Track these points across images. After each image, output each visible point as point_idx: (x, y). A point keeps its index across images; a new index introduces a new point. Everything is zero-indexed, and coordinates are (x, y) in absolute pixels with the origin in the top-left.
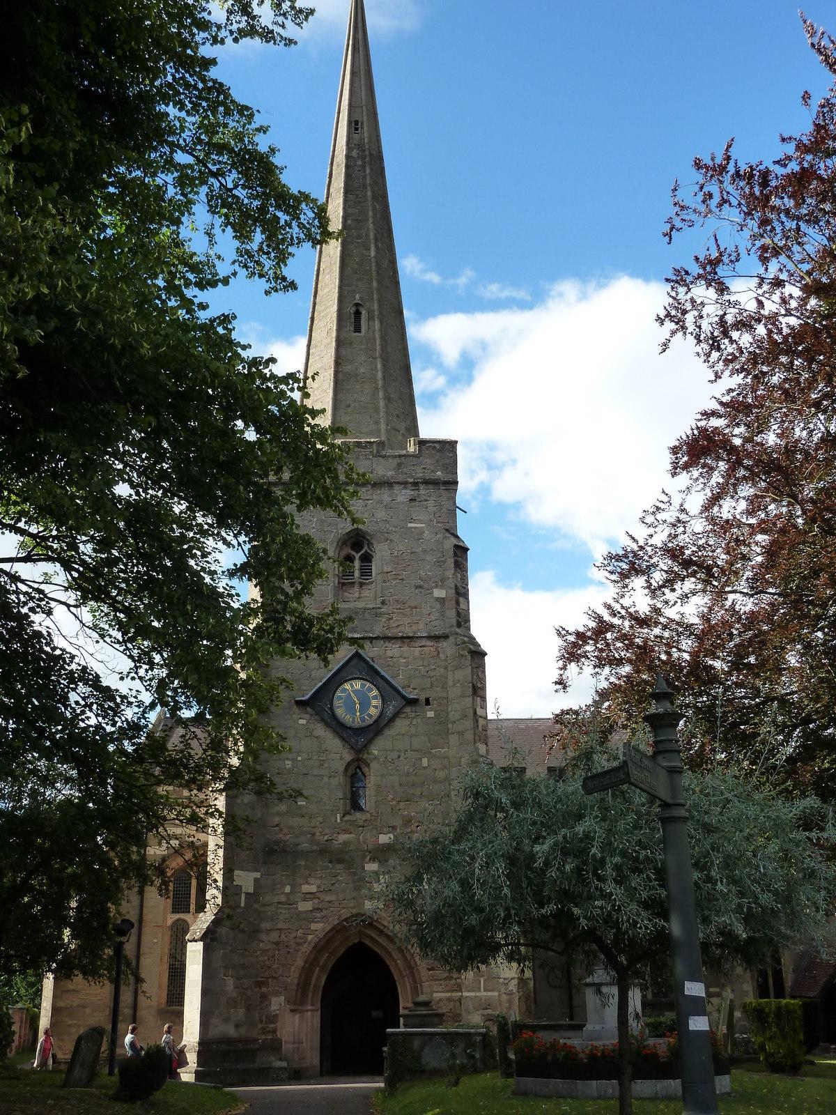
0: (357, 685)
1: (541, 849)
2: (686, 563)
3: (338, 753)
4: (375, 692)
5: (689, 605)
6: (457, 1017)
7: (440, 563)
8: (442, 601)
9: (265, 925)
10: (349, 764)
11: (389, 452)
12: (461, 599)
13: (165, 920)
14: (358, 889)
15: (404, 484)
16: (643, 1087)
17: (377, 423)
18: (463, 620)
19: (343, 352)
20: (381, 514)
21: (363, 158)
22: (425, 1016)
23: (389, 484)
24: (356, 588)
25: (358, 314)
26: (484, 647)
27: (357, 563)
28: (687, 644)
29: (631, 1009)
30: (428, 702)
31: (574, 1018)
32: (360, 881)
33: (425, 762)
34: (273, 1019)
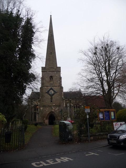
3: (50, 97)
32: (52, 108)
34: (44, 120)
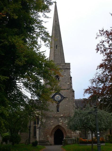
0: (58, 95)
1: (83, 118)
5: (101, 86)
6: (71, 138)
7: (68, 79)
9: (46, 126)
10: (57, 106)
11: (61, 65)
13: (33, 126)
14: (58, 122)
15: (63, 69)
16: (94, 145)
18: (71, 87)
19: (55, 52)
21: (57, 26)
25: (57, 46)
26: (74, 90)
27: (57, 80)
28: (101, 91)
29: (93, 136)
30: (67, 98)
31: (86, 137)
32: (59, 121)
33: (67, 105)
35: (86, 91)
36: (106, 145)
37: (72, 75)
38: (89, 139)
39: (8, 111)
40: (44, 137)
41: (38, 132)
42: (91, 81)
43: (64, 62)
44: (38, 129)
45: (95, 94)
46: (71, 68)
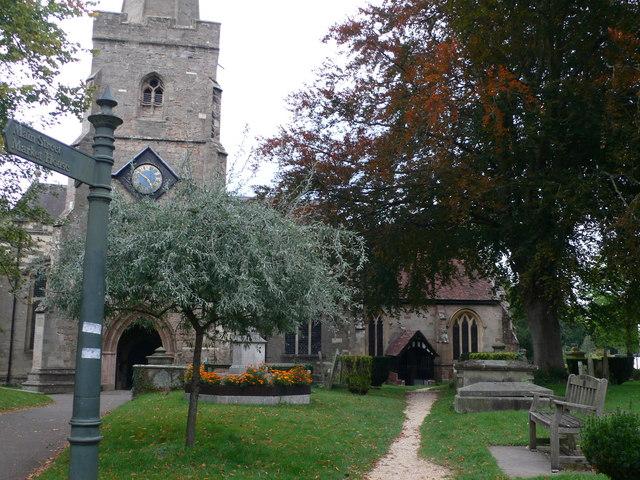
0: (148, 167)
2: (347, 108)
4: (158, 173)
5: (340, 130)
7: (204, 98)
8: (203, 120)
12: (215, 121)
15: (186, 47)
17: (173, 8)
18: (215, 133)
20: (170, 65)
22: (161, 358)
23: (177, 46)
24: (152, 109)
26: (227, 151)
27: (153, 94)
35: (269, 147)
36: (313, 404)
37: (222, 79)
38: (236, 371)
39: (595, 403)
40: (69, 353)
41: (39, 330)
42: (292, 100)
43: (192, 14)
44: (43, 316)
45: (316, 177)
46: (220, 47)
